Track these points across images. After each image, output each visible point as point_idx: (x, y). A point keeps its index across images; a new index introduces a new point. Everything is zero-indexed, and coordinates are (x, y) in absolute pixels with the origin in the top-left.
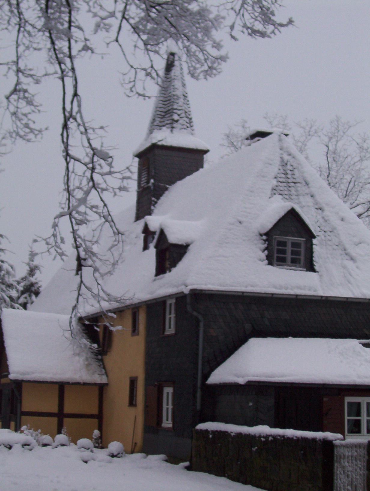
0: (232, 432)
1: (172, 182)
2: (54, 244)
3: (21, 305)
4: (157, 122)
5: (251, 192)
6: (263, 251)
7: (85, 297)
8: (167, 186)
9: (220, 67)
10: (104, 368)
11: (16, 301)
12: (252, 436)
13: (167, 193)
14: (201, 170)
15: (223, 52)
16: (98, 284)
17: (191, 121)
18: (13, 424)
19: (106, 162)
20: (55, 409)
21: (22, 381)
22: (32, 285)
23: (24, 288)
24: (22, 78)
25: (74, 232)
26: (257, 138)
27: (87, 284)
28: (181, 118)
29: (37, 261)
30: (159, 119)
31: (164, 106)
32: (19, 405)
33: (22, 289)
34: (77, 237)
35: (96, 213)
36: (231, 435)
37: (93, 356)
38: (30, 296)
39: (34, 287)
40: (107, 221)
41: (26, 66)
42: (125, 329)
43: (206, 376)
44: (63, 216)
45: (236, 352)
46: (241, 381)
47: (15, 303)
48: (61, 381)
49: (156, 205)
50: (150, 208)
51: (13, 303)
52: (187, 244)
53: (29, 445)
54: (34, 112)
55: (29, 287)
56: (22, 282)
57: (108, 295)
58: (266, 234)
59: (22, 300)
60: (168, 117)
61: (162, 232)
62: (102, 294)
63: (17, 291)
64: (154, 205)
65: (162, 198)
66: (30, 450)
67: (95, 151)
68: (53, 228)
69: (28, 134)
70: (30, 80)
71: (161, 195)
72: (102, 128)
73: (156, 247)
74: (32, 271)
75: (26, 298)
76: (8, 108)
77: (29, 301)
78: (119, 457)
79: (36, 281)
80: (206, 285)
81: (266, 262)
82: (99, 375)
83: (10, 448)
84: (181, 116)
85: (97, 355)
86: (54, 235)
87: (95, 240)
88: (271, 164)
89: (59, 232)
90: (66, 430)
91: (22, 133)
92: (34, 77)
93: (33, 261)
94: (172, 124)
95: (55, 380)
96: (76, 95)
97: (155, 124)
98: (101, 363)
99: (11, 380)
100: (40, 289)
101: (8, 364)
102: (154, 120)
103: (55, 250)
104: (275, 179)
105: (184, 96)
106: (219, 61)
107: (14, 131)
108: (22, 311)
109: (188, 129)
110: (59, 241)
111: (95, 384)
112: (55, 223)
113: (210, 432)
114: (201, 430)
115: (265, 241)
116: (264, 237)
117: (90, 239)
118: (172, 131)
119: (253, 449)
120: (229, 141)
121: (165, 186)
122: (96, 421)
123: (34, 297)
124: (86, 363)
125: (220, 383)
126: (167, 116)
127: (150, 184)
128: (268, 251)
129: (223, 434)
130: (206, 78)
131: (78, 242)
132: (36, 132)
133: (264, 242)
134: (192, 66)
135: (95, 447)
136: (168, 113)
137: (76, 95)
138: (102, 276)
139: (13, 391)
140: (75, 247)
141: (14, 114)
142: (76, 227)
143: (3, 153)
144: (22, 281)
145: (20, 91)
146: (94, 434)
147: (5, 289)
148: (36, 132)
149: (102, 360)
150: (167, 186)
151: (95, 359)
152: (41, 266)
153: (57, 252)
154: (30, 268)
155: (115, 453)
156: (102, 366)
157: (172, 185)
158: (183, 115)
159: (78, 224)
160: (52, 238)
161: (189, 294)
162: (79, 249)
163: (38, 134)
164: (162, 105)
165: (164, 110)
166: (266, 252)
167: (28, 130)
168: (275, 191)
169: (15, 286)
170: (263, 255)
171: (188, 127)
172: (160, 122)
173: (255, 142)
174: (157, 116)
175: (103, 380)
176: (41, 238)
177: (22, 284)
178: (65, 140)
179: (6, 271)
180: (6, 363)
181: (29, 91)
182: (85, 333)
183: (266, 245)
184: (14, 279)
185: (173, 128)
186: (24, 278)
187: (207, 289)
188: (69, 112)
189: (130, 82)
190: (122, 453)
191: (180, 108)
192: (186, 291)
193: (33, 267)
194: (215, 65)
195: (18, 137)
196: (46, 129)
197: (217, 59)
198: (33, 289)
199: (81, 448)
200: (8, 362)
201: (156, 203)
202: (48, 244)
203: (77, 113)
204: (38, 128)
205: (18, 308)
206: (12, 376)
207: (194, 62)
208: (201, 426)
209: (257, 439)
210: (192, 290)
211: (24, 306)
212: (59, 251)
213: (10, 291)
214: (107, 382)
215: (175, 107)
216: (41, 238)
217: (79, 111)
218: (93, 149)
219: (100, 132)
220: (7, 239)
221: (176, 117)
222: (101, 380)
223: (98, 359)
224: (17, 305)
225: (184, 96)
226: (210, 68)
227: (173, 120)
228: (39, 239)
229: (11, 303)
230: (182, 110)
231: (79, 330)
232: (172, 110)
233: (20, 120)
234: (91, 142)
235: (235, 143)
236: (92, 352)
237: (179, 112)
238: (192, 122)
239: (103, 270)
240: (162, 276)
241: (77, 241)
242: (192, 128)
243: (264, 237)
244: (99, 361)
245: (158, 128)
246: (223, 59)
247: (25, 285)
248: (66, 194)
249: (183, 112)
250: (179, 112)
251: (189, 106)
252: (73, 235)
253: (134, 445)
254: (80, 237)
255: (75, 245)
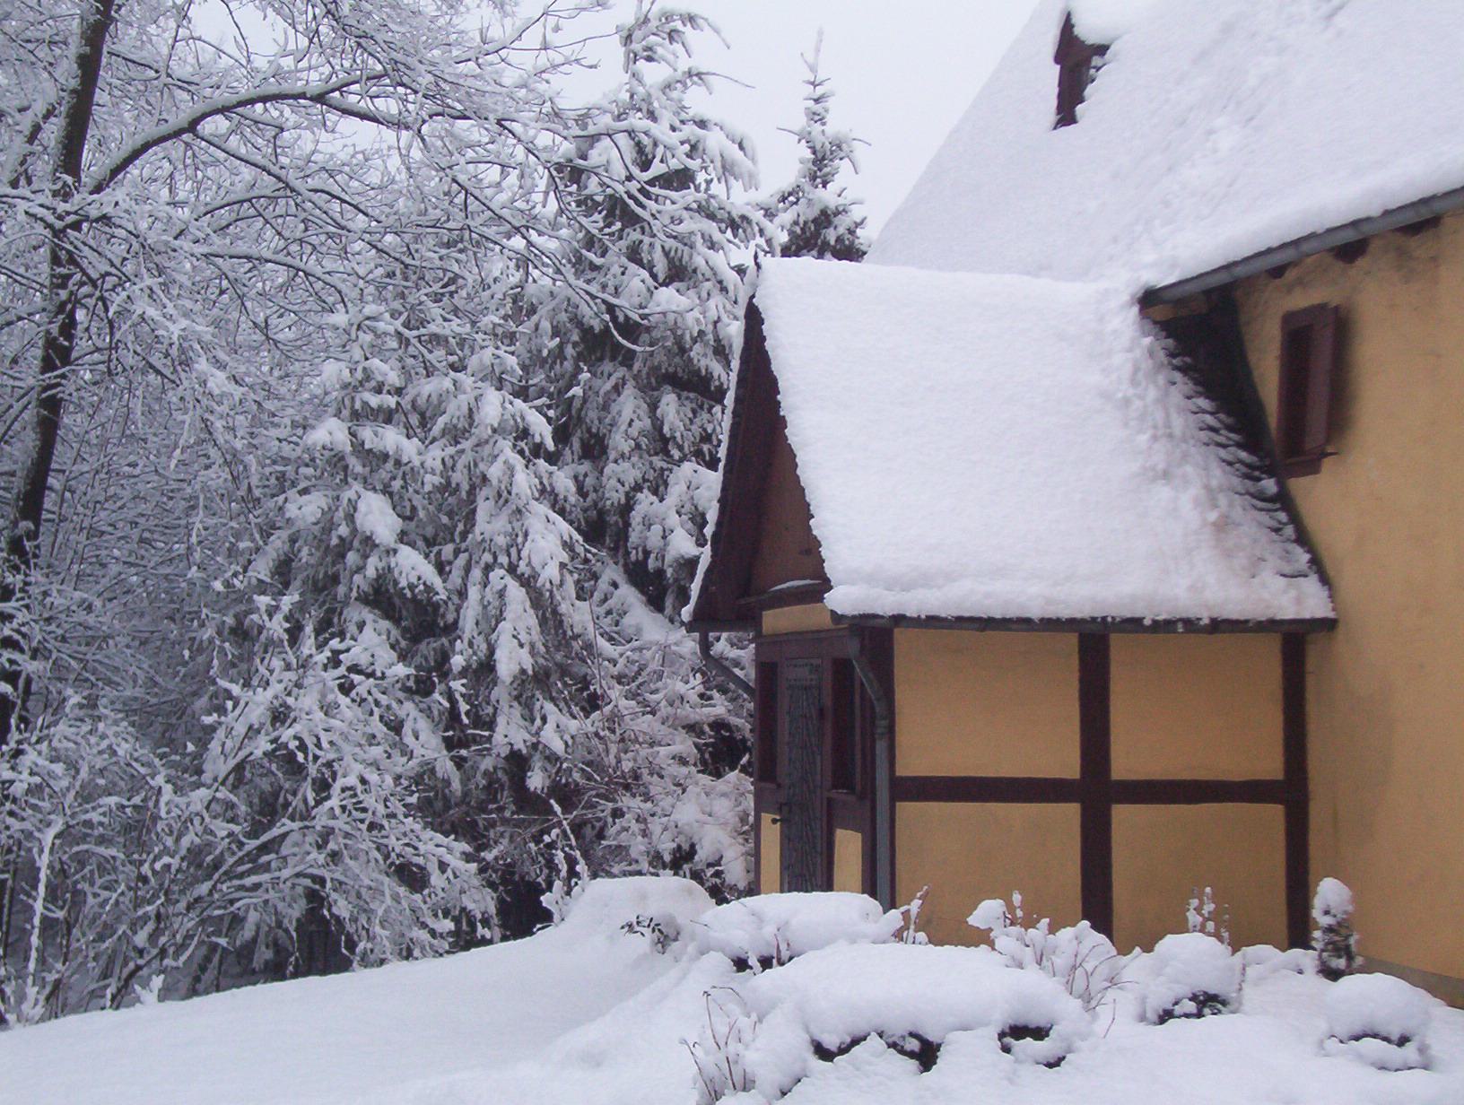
10: (1303, 539)
20: (1065, 762)
21: (899, 620)
22: (825, 218)
32: (881, 746)
37: (1236, 481)
48: (1098, 614)
53: (1039, 1033)
66: (1050, 1065)
74: (820, 165)
79: (841, 201)
82: (1284, 575)
83: (926, 1054)
85: (1257, 473)
90: (1209, 907)
95: (1065, 613)
98: (1283, 516)
111: (1270, 625)
122: (1273, 815)
124: (1213, 516)
139: (842, 668)
147: (717, 236)
149: (1284, 501)
151: (1253, 496)
156: (1289, 531)
175: (1309, 601)
177: (787, 217)
182: (1183, 369)
186: (790, 194)
198: (831, 236)
199: (1357, 1038)
206: (844, 598)
214: (1331, 615)
220: (717, 31)
222: (1298, 601)
231: (1151, 354)
236: (1230, 464)
244: (1269, 505)
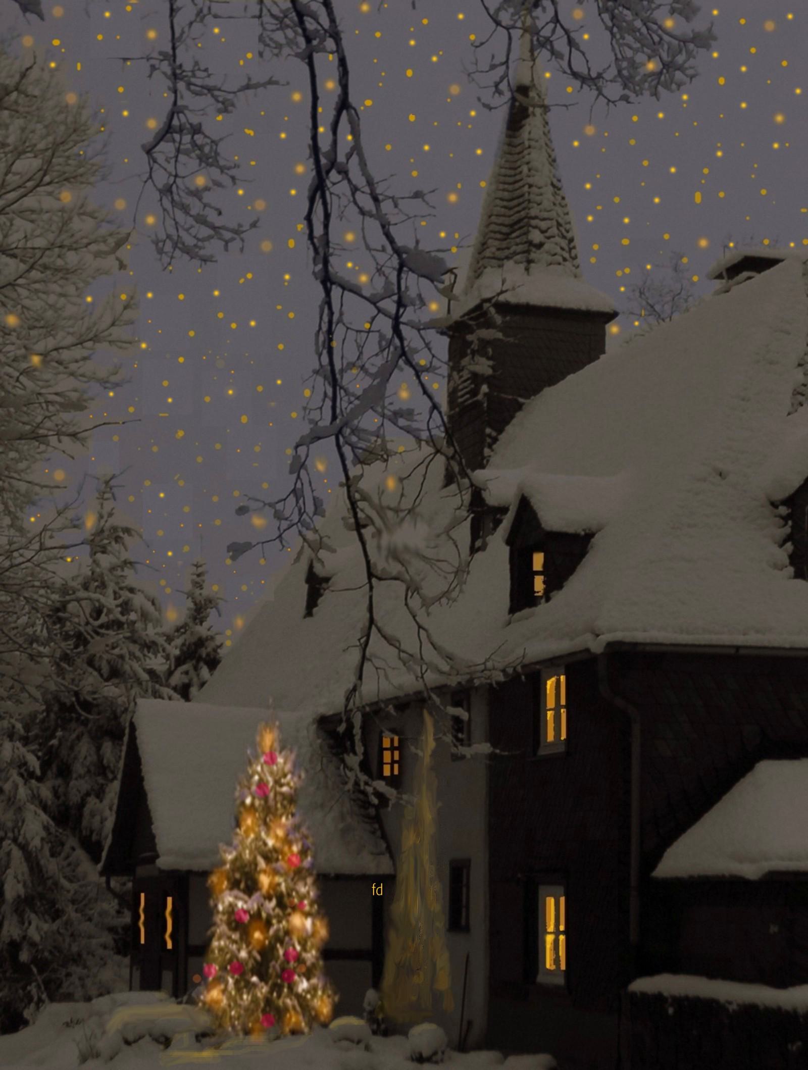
0: (730, 1003)
1: (533, 390)
2: (295, 518)
3: (175, 689)
4: (493, 249)
5: (743, 399)
6: (781, 545)
7: (378, 663)
8: (521, 400)
9: (691, 62)
10: (384, 837)
11: (164, 680)
12: (787, 1012)
13: (519, 415)
14: (602, 357)
15: (699, 25)
16: (420, 627)
17: (572, 245)
18: (167, 977)
19: (436, 287)
22: (201, 642)
23: (181, 650)
24: (187, 99)
25: (349, 483)
26: (745, 274)
27: (389, 630)
28: (549, 238)
29: (212, 588)
30: (497, 243)
31: (507, 210)
33: (177, 652)
34: (357, 496)
35: (408, 430)
36: (727, 1010)
38: (196, 668)
39: (206, 648)
40: (438, 451)
41: (196, 63)
42: (498, 751)
43: (654, 857)
44: (319, 438)
45: (727, 798)
46: (751, 871)
47: (161, 685)
49: (494, 446)
50: (481, 453)
51: (157, 686)
52: (587, 531)
54: (218, 184)
55: (193, 647)
56: (178, 637)
57: (450, 659)
58: (789, 501)
59: (177, 678)
60: (517, 237)
61: (524, 504)
62: (429, 654)
63: (167, 658)
64: (490, 446)
65: (509, 429)
67: (404, 256)
68: (291, 472)
69: (206, 244)
70: (206, 101)
71: (506, 421)
72: (418, 195)
73: (509, 542)
74: (199, 612)
75: (187, 673)
76: (151, 177)
77: (195, 680)
78: (436, 1062)
79: (209, 633)
80: (645, 631)
81: (791, 570)
84: (547, 234)
86: (297, 493)
87: (407, 504)
88: (788, 333)
89: (310, 482)
91: (189, 241)
92: (216, 93)
93: (201, 587)
94: (528, 252)
96: (344, 104)
97: (488, 253)
99: (161, 871)
100: (219, 651)
101: (154, 831)
102: (484, 245)
103: (300, 533)
104: (800, 368)
105: (553, 185)
106: (691, 46)
107: (169, 237)
108: (179, 703)
109: (567, 263)
110: (310, 508)
112: (296, 457)
113: (670, 1000)
114: (644, 995)
115: (785, 519)
116: (783, 510)
117: (393, 504)
118: (527, 269)
119: (790, 1046)
120: (644, 303)
121: (516, 401)
123: (205, 671)
124: (341, 826)
125: (691, 877)
126: (514, 235)
127: (480, 397)
128: (793, 544)
129: (711, 1006)
130: (655, 94)
131: (362, 510)
132: (228, 235)
133: (782, 522)
134: (624, 58)
135: (374, 1033)
136: (516, 227)
137: (344, 104)
138: (426, 603)
140: (354, 526)
141: (167, 190)
142: (354, 471)
143: (125, 342)
144: (176, 634)
145: (181, 130)
146: (366, 1001)
147: (138, 654)
148: (228, 235)
150: (521, 400)
152: (218, 598)
153: (305, 540)
154: (196, 604)
155: (426, 1054)
156: (379, 833)
157: (533, 397)
158: (554, 231)
159: (359, 461)
160: (292, 499)
161: (602, 654)
162: (363, 531)
163: (233, 239)
164: (503, 210)
165: (507, 221)
166: (789, 546)
167: (205, 231)
168: (800, 398)
169: (162, 645)
170: (782, 555)
171: (565, 260)
172: (498, 249)
173: (739, 283)
174: (492, 235)
176: (258, 500)
177: (178, 641)
178: (318, 231)
179: (139, 611)
180: (151, 830)
181: (205, 128)
183: (788, 530)
184: (159, 630)
185: (529, 262)
186: (182, 627)
187: (648, 641)
188: (326, 155)
189: (493, 67)
190: (443, 1053)
191: (546, 215)
192: (597, 646)
193: (203, 602)
194: (680, 59)
195: (178, 253)
196: (254, 225)
197: (684, 42)
198: (203, 652)
199: (340, 1040)
200: (153, 827)
201: (495, 440)
202: (278, 516)
203: (349, 156)
204: (233, 225)
205: (170, 698)
207: (630, 47)
208: (643, 985)
209: (801, 1020)
210: (610, 645)
211: (184, 692)
212: (310, 535)
213: (150, 659)
215: (533, 212)
216: (258, 500)
217: (356, 148)
218: (397, 251)
219: (410, 206)
221: (536, 236)
223: (368, 816)
224: (166, 691)
225: (553, 185)
226: (665, 65)
227: (530, 243)
228: (253, 505)
229: (153, 687)
230: (552, 219)
232: (526, 220)
233: (185, 209)
234: (393, 230)
235: (657, 308)
236: (354, 800)
237: (543, 225)
238: (574, 248)
239: (433, 585)
240: (526, 611)
241: (358, 510)
242: (576, 262)
243: (783, 510)
245: (494, 262)
246: (703, 40)
247: (183, 645)
248: (323, 385)
249: (555, 223)
250: (543, 225)
251: (566, 210)
252: (349, 492)
253: (465, 1023)
254: (364, 498)
255: (352, 520)
